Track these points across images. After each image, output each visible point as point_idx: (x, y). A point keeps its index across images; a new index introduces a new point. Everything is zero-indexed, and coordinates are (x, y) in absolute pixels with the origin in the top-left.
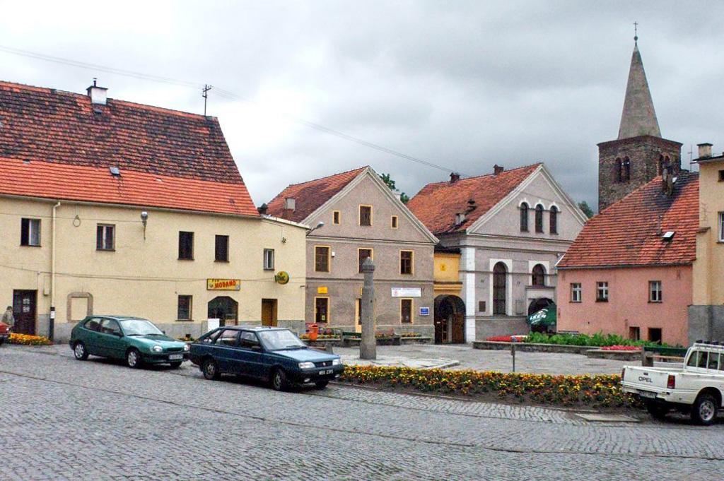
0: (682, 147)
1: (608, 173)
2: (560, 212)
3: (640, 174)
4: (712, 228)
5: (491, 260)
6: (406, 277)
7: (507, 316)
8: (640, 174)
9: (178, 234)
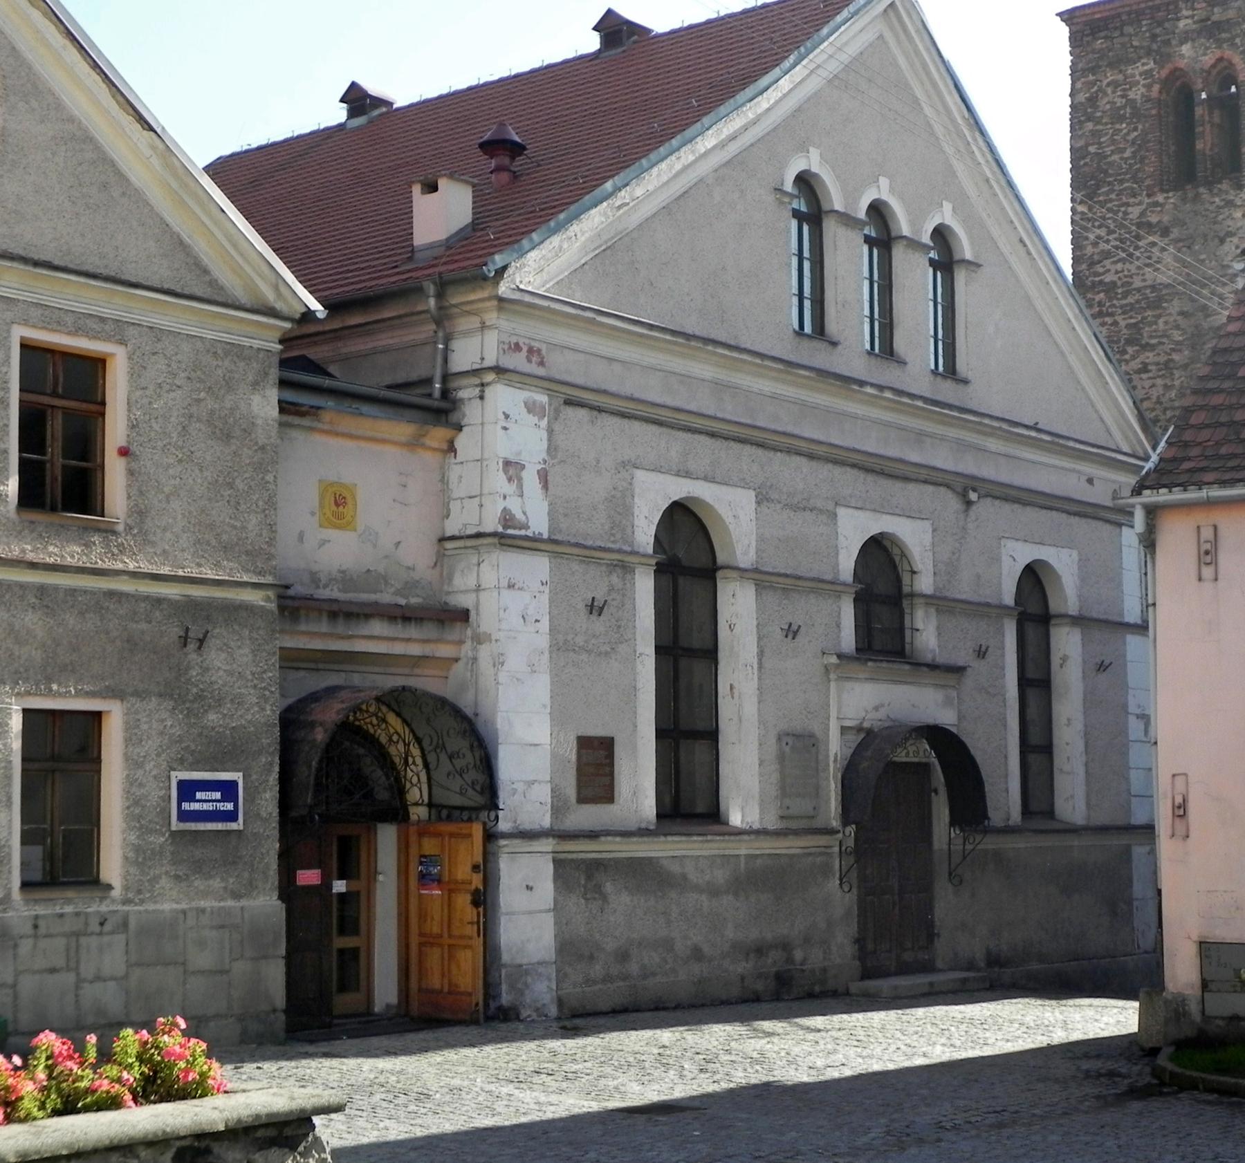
4: (909, 367)
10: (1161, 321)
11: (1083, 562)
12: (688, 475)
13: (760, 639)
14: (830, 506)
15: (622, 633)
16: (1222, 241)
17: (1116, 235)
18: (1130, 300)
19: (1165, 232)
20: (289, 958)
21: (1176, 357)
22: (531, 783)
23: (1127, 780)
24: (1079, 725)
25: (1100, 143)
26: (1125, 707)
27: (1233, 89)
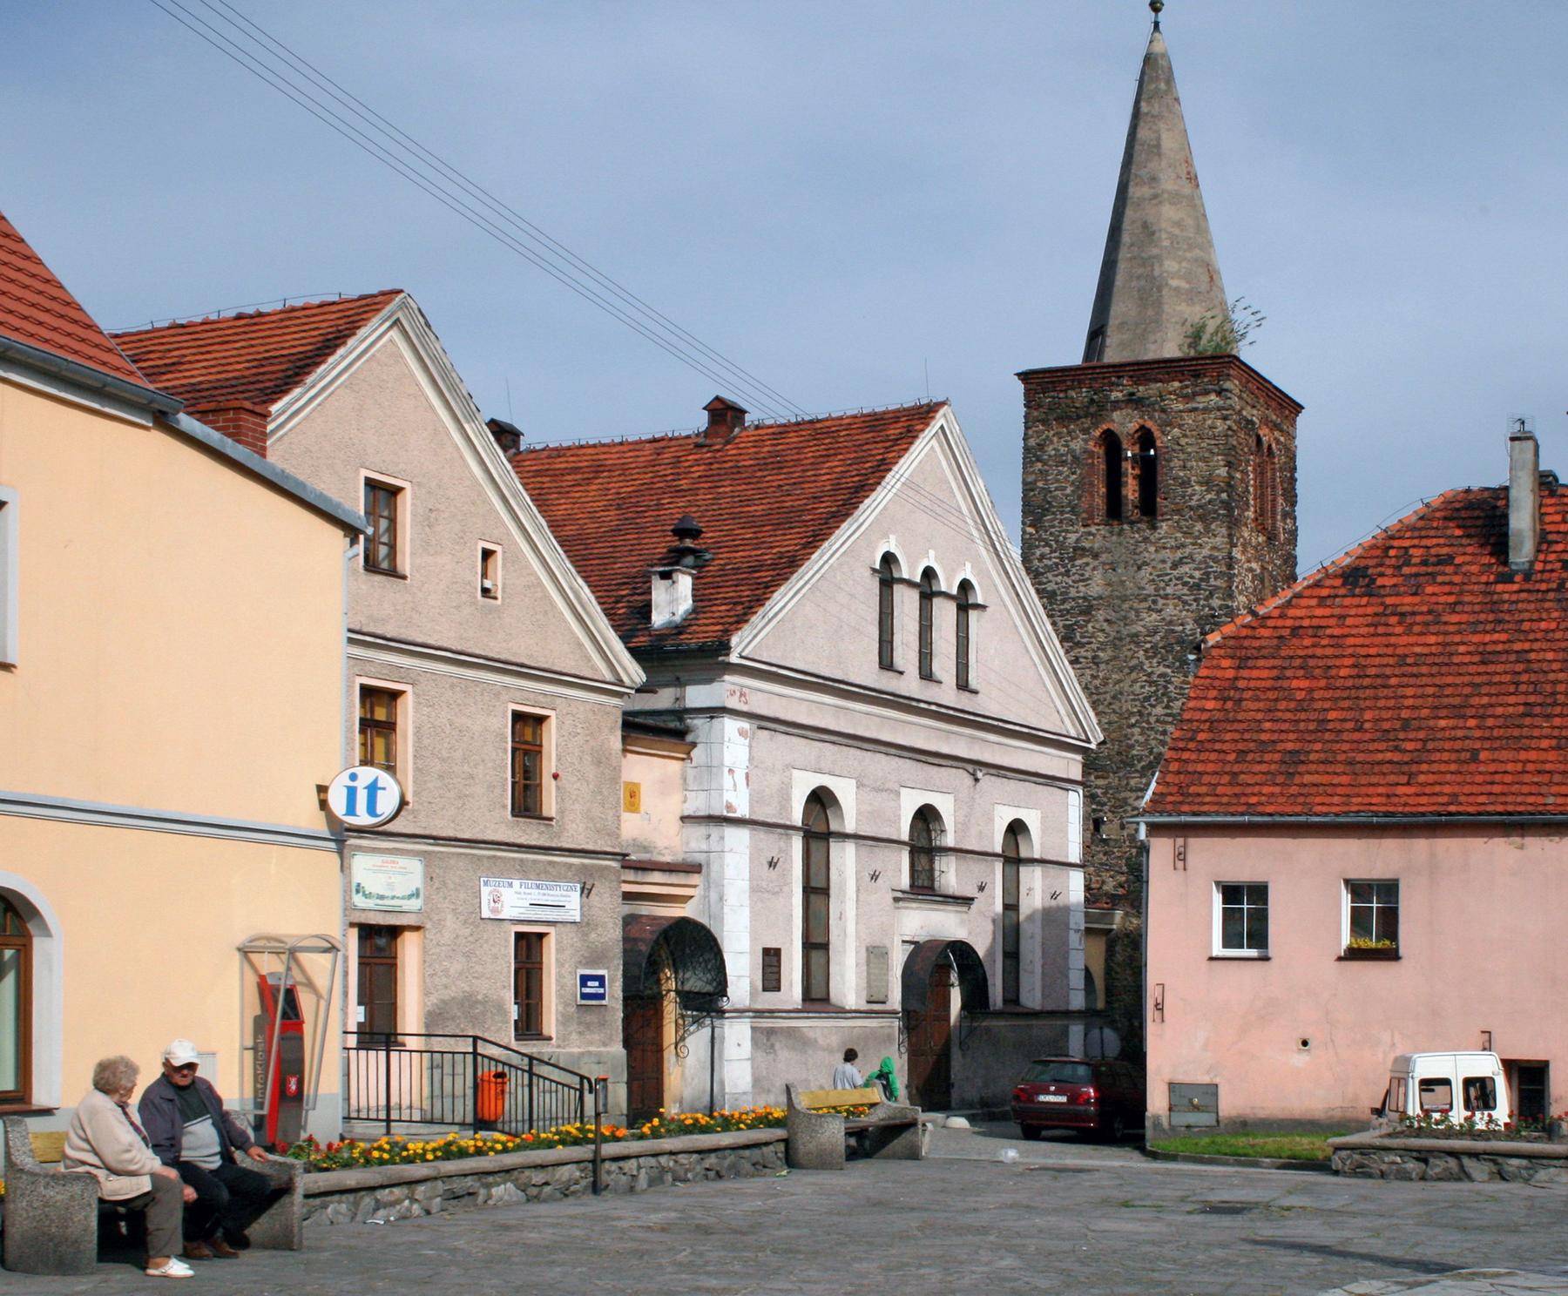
1: (1063, 482)
2: (982, 607)
5: (999, 808)
6: (528, 832)
8: (1199, 494)
9: (1541, 1057)
10: (1090, 625)
11: (1044, 819)
13: (857, 880)
14: (896, 787)
16: (1139, 568)
17: (1057, 554)
18: (1067, 606)
19: (1096, 556)
20: (629, 1083)
21: (1101, 654)
24: (1038, 938)
25: (1046, 480)
26: (1067, 925)
27: (1152, 452)
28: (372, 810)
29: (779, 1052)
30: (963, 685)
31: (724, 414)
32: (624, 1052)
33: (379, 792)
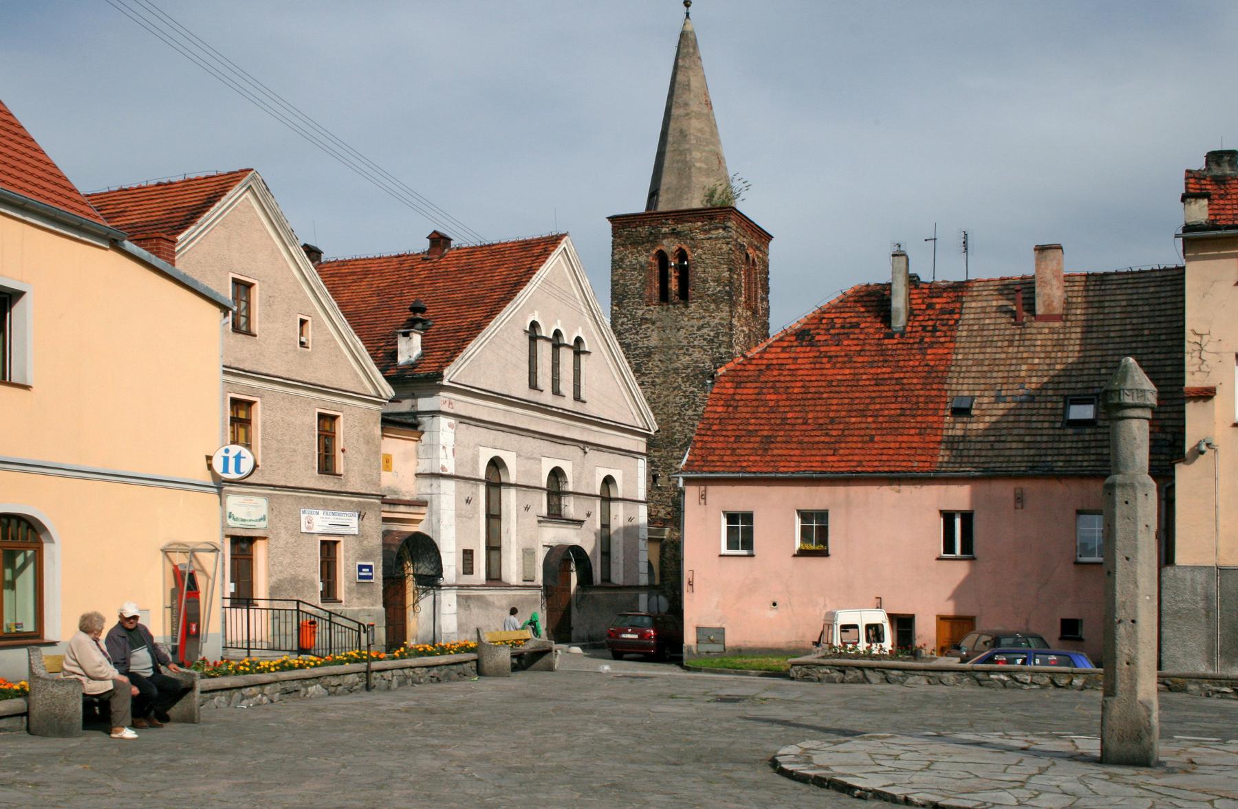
0: (771, 244)
1: (635, 281)
3: (713, 287)
7: (508, 586)
8: (713, 287)
10: (650, 364)
11: (624, 475)
12: (495, 448)
14: (539, 457)
15: (476, 509)
16: (679, 330)
18: (637, 352)
19: (653, 323)
20: (386, 627)
21: (656, 380)
22: (449, 566)
23: (638, 566)
24: (621, 544)
26: (638, 536)
27: (686, 263)
28: (237, 470)
29: (473, 610)
30: (577, 398)
31: (439, 241)
32: (383, 609)
33: (242, 460)
